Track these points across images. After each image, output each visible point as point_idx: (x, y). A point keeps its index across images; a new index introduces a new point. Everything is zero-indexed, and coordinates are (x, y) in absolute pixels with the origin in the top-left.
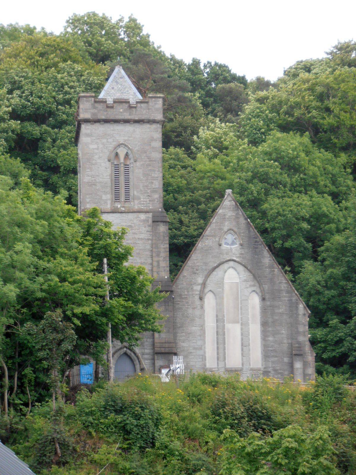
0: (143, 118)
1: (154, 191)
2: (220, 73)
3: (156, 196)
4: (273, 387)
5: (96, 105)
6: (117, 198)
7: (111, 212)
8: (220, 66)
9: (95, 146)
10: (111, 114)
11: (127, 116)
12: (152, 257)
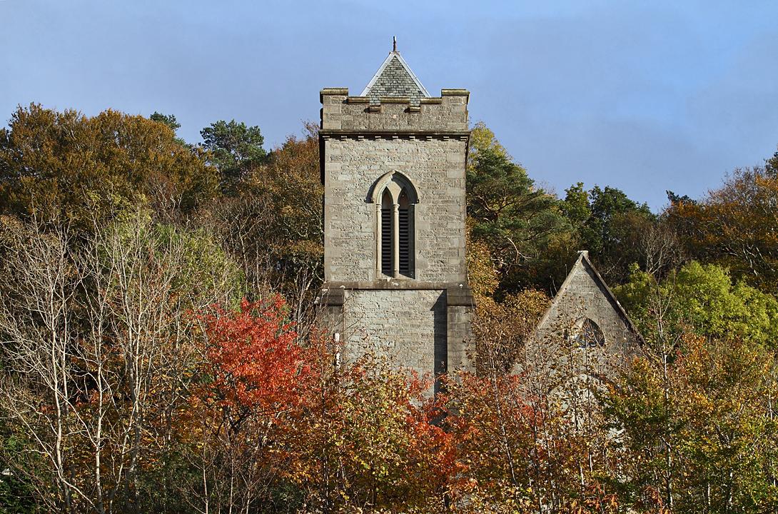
0: (433, 129)
1: (452, 253)
2: (610, 201)
3: (455, 262)
4: (79, 459)
5: (351, 107)
6: (388, 268)
7: (373, 289)
8: (612, 192)
9: (348, 178)
10: (376, 123)
11: (404, 127)
12: (358, 289)
